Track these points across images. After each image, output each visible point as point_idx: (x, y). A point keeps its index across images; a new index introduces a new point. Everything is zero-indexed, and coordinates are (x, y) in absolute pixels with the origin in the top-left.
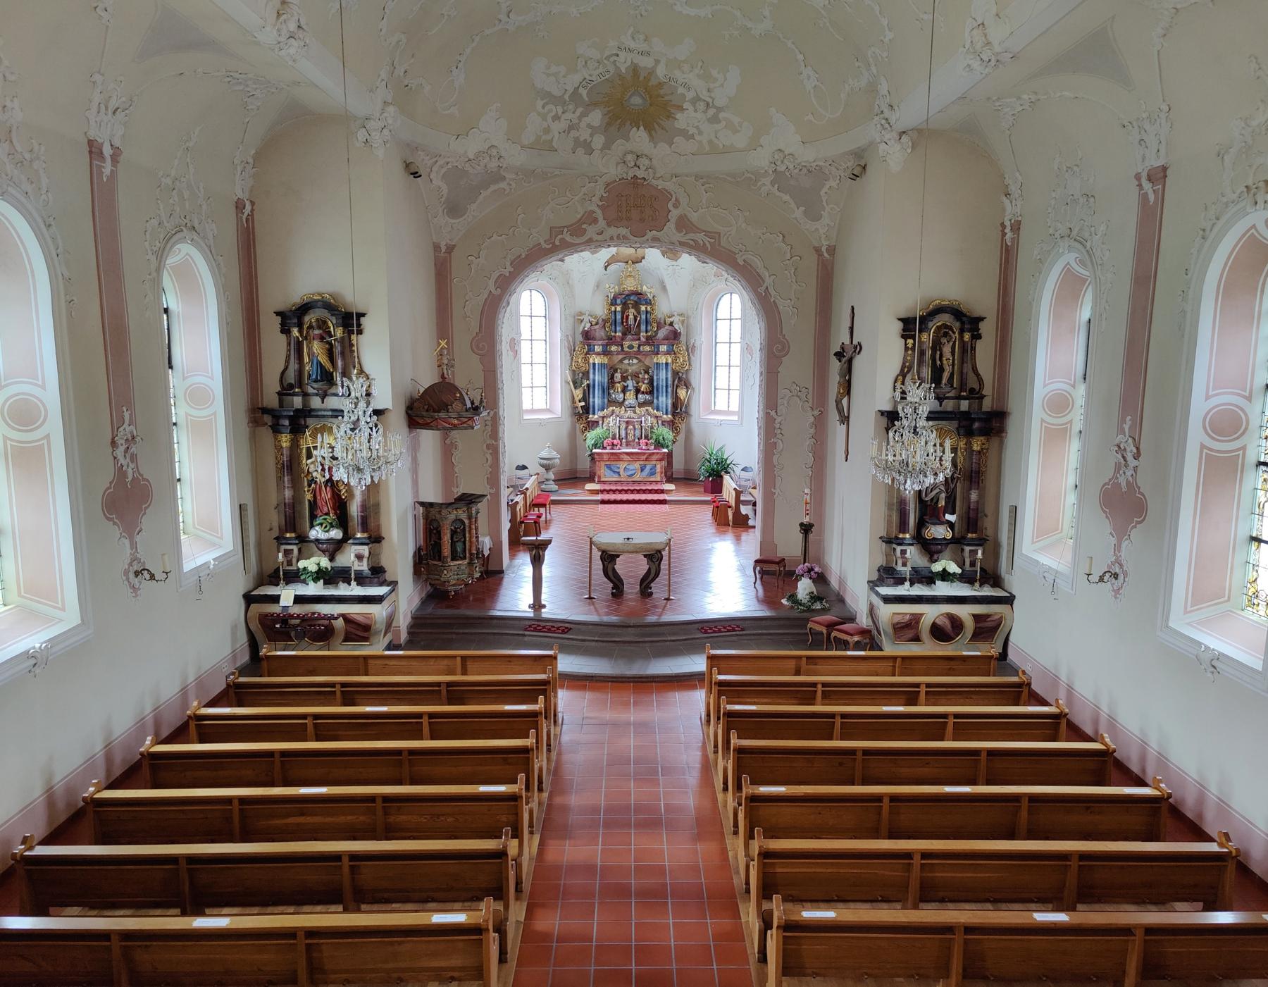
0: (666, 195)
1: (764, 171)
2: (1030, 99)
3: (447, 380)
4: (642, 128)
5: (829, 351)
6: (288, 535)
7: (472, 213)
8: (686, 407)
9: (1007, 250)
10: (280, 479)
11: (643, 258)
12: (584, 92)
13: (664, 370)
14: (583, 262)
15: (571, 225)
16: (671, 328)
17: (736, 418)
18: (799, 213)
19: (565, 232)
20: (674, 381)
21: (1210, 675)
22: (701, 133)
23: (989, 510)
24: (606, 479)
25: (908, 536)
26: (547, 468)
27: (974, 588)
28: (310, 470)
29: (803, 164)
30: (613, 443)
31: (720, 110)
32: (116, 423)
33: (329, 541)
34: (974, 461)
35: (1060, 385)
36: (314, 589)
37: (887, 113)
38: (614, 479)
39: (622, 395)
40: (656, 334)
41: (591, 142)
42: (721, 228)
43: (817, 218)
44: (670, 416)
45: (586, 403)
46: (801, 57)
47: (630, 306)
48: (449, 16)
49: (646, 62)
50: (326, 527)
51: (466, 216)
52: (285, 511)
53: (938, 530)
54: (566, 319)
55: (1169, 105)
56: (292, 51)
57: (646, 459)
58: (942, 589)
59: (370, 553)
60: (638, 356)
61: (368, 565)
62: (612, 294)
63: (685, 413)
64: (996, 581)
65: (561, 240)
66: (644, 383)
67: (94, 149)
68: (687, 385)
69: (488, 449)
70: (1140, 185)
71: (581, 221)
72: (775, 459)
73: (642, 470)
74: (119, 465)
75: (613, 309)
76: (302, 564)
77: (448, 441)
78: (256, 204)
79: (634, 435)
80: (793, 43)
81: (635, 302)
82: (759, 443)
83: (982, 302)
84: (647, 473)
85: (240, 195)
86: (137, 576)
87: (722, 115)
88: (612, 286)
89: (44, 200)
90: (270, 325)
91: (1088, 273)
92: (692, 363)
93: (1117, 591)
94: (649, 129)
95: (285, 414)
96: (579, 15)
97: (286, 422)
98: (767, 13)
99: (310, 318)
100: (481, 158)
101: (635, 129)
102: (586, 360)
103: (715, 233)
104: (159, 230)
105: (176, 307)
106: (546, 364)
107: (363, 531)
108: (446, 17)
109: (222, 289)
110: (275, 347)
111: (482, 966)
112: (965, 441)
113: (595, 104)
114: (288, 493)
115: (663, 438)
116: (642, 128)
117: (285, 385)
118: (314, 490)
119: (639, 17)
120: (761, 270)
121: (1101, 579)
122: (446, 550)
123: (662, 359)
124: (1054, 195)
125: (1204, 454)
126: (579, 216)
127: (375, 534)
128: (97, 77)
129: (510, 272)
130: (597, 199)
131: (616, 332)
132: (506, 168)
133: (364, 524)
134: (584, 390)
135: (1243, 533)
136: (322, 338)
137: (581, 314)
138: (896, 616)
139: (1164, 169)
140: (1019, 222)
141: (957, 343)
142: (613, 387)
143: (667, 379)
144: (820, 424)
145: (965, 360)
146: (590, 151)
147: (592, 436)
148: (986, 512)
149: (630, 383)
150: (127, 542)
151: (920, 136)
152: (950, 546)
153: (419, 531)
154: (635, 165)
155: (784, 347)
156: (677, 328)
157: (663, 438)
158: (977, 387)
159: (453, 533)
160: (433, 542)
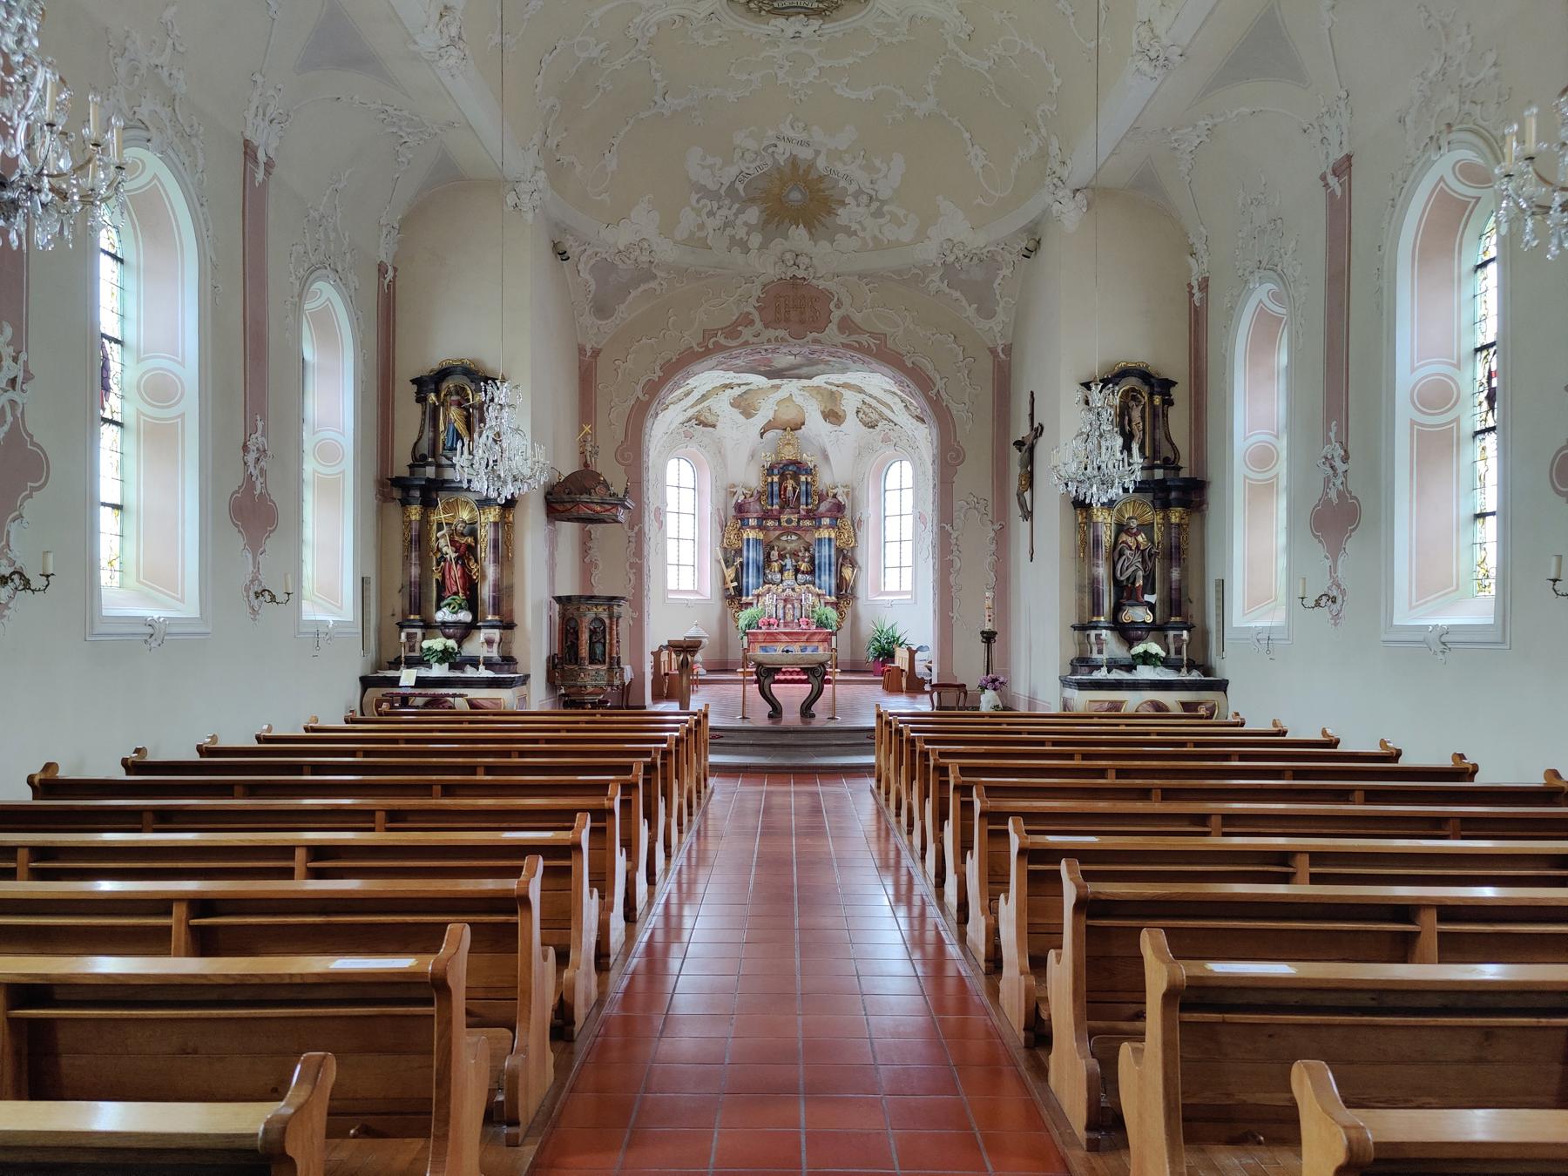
0: (827, 296)
1: (931, 265)
2: (1207, 124)
3: (590, 468)
4: (801, 226)
5: (1009, 438)
6: (412, 617)
7: (620, 314)
8: (852, 589)
9: (1196, 310)
10: (407, 558)
11: (803, 424)
12: (740, 187)
13: (827, 546)
15: (726, 327)
16: (834, 500)
18: (971, 311)
19: (719, 335)
20: (837, 560)
21: (1440, 656)
22: (864, 229)
23: (1194, 594)
25: (1102, 619)
27: (1181, 674)
28: (440, 546)
29: (974, 251)
31: (883, 202)
32: (250, 429)
33: (456, 624)
34: (1173, 535)
35: (1261, 437)
36: (439, 671)
37: (1059, 170)
39: (779, 576)
40: (818, 508)
41: (747, 240)
42: (888, 329)
43: (990, 315)
44: (834, 598)
45: (739, 583)
46: (967, 135)
47: (789, 476)
48: (604, 89)
49: (805, 154)
50: (454, 608)
51: (614, 318)
52: (411, 591)
53: (1137, 612)
54: (717, 491)
55: (1346, 91)
56: (452, 61)
57: (807, 641)
58: (1145, 673)
59: (501, 639)
61: (498, 652)
62: (769, 463)
64: (1207, 670)
65: (716, 343)
67: (249, 151)
68: (853, 564)
69: (631, 568)
70: (1326, 185)
71: (736, 324)
72: (952, 579)
74: (249, 473)
75: (770, 480)
76: (426, 644)
77: (586, 560)
78: (400, 269)
80: (959, 121)
81: (795, 472)
82: (934, 564)
83: (1172, 364)
85: (383, 257)
86: (257, 597)
87: (886, 208)
89: (199, 179)
90: (405, 394)
91: (1284, 311)
92: (858, 540)
93: (1336, 616)
94: (809, 227)
95: (417, 483)
96: (736, 100)
97: (417, 494)
98: (930, 89)
99: (449, 384)
100: (631, 250)
101: (794, 226)
102: (739, 536)
103: (882, 334)
104: (304, 259)
105: (311, 358)
106: (694, 540)
107: (494, 614)
108: (601, 90)
109: (360, 346)
110: (409, 416)
111: (631, 840)
112: (1162, 514)
113: (752, 200)
114: (415, 571)
115: (826, 617)
116: (801, 226)
117: (418, 457)
118: (443, 570)
119: (798, 102)
120: (932, 373)
121: (1318, 604)
122: (584, 651)
123: (825, 534)
124: (1240, 235)
125: (1415, 430)
126: (735, 318)
127: (507, 619)
128: (260, 79)
129: (659, 377)
130: (753, 301)
132: (658, 264)
133: (497, 609)
134: (737, 569)
135: (1466, 513)
136: (459, 405)
137: (734, 486)
138: (1093, 704)
139: (1349, 157)
140: (1206, 280)
141: (1147, 410)
142: (769, 566)
143: (830, 556)
144: (1002, 538)
145: (1157, 425)
146: (746, 250)
147: (745, 616)
148: (1191, 596)
149: (789, 562)
150: (250, 556)
151: (1095, 194)
152: (1151, 633)
153: (555, 635)
154: (794, 264)
155: (958, 457)
156: (841, 500)
157: (826, 617)
158: (1171, 455)
159: (593, 632)
160: (569, 643)
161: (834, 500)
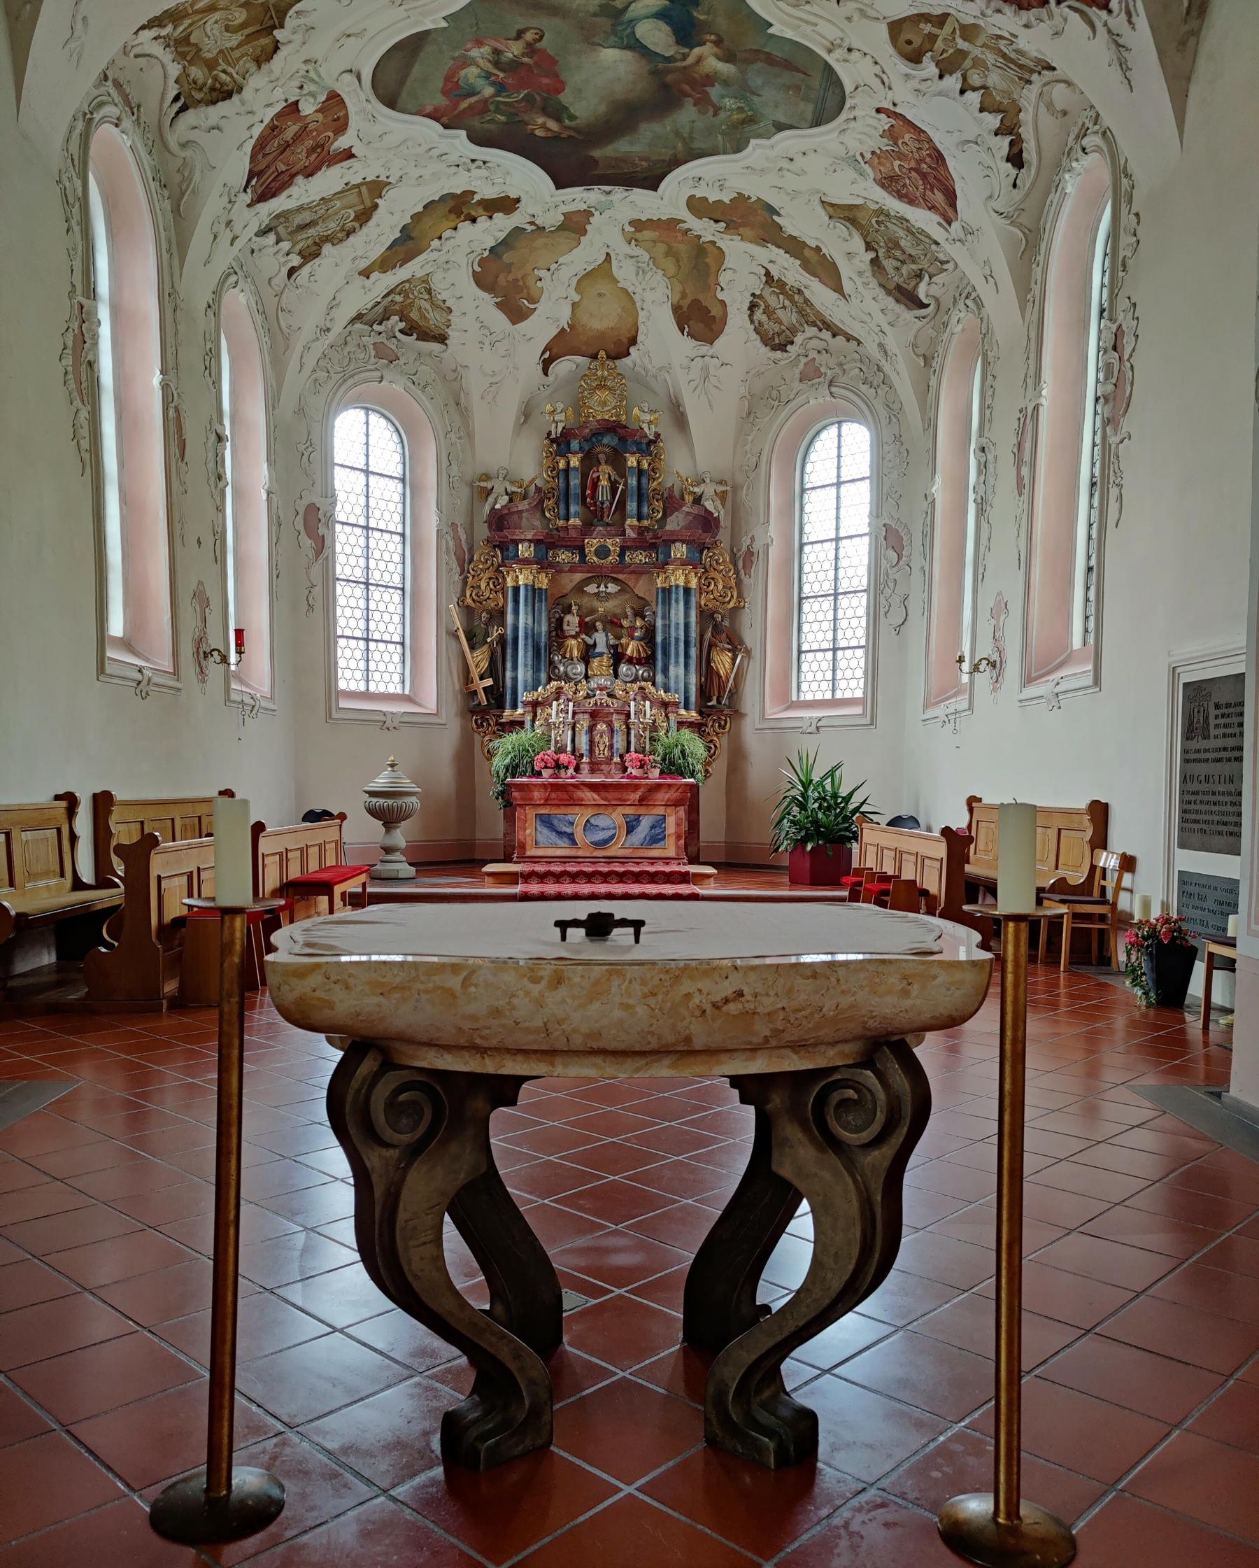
11: (633, 341)
14: (492, 345)
17: (858, 710)
20: (702, 636)
24: (540, 852)
26: (389, 819)
30: (557, 761)
38: (559, 852)
39: (580, 668)
54: (452, 487)
57: (642, 802)
60: (621, 577)
63: (729, 707)
66: (633, 639)
68: (735, 645)
73: (630, 829)
75: (562, 465)
79: (611, 747)
81: (614, 449)
84: (642, 836)
88: (560, 406)
92: (745, 595)
115: (683, 752)
131: (568, 520)
137: (486, 477)
142: (561, 645)
149: (601, 640)
161: (695, 510)
